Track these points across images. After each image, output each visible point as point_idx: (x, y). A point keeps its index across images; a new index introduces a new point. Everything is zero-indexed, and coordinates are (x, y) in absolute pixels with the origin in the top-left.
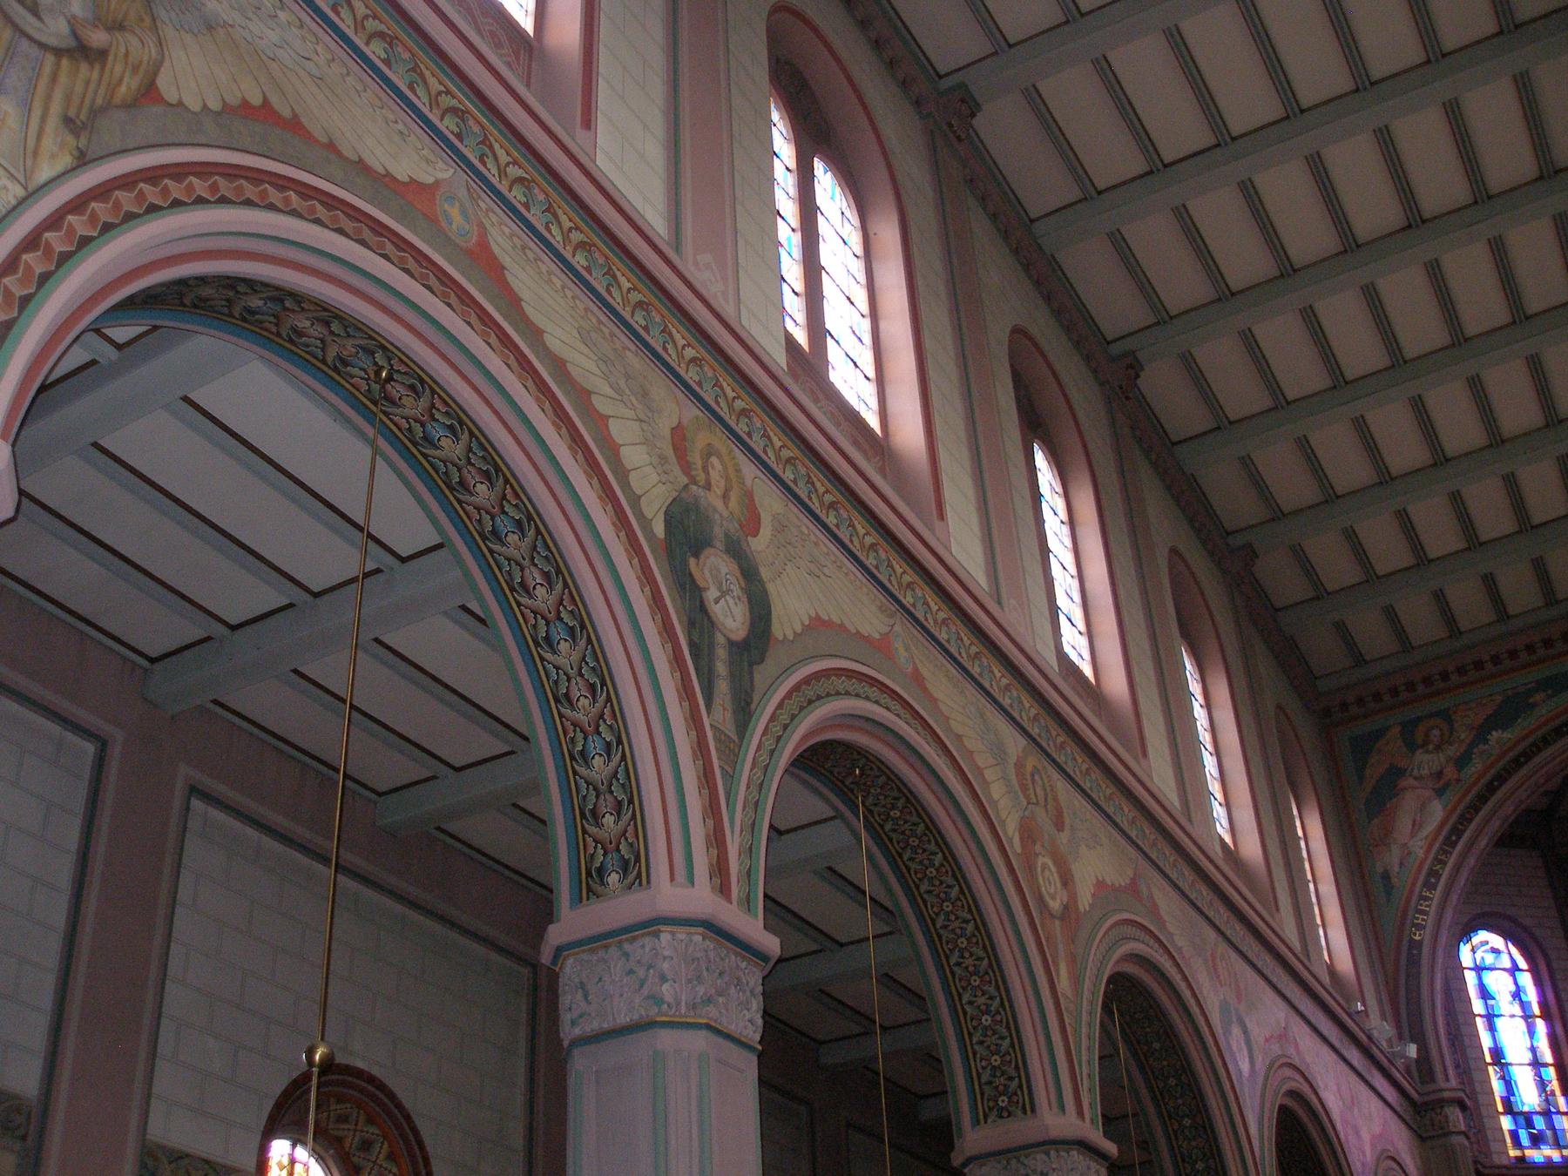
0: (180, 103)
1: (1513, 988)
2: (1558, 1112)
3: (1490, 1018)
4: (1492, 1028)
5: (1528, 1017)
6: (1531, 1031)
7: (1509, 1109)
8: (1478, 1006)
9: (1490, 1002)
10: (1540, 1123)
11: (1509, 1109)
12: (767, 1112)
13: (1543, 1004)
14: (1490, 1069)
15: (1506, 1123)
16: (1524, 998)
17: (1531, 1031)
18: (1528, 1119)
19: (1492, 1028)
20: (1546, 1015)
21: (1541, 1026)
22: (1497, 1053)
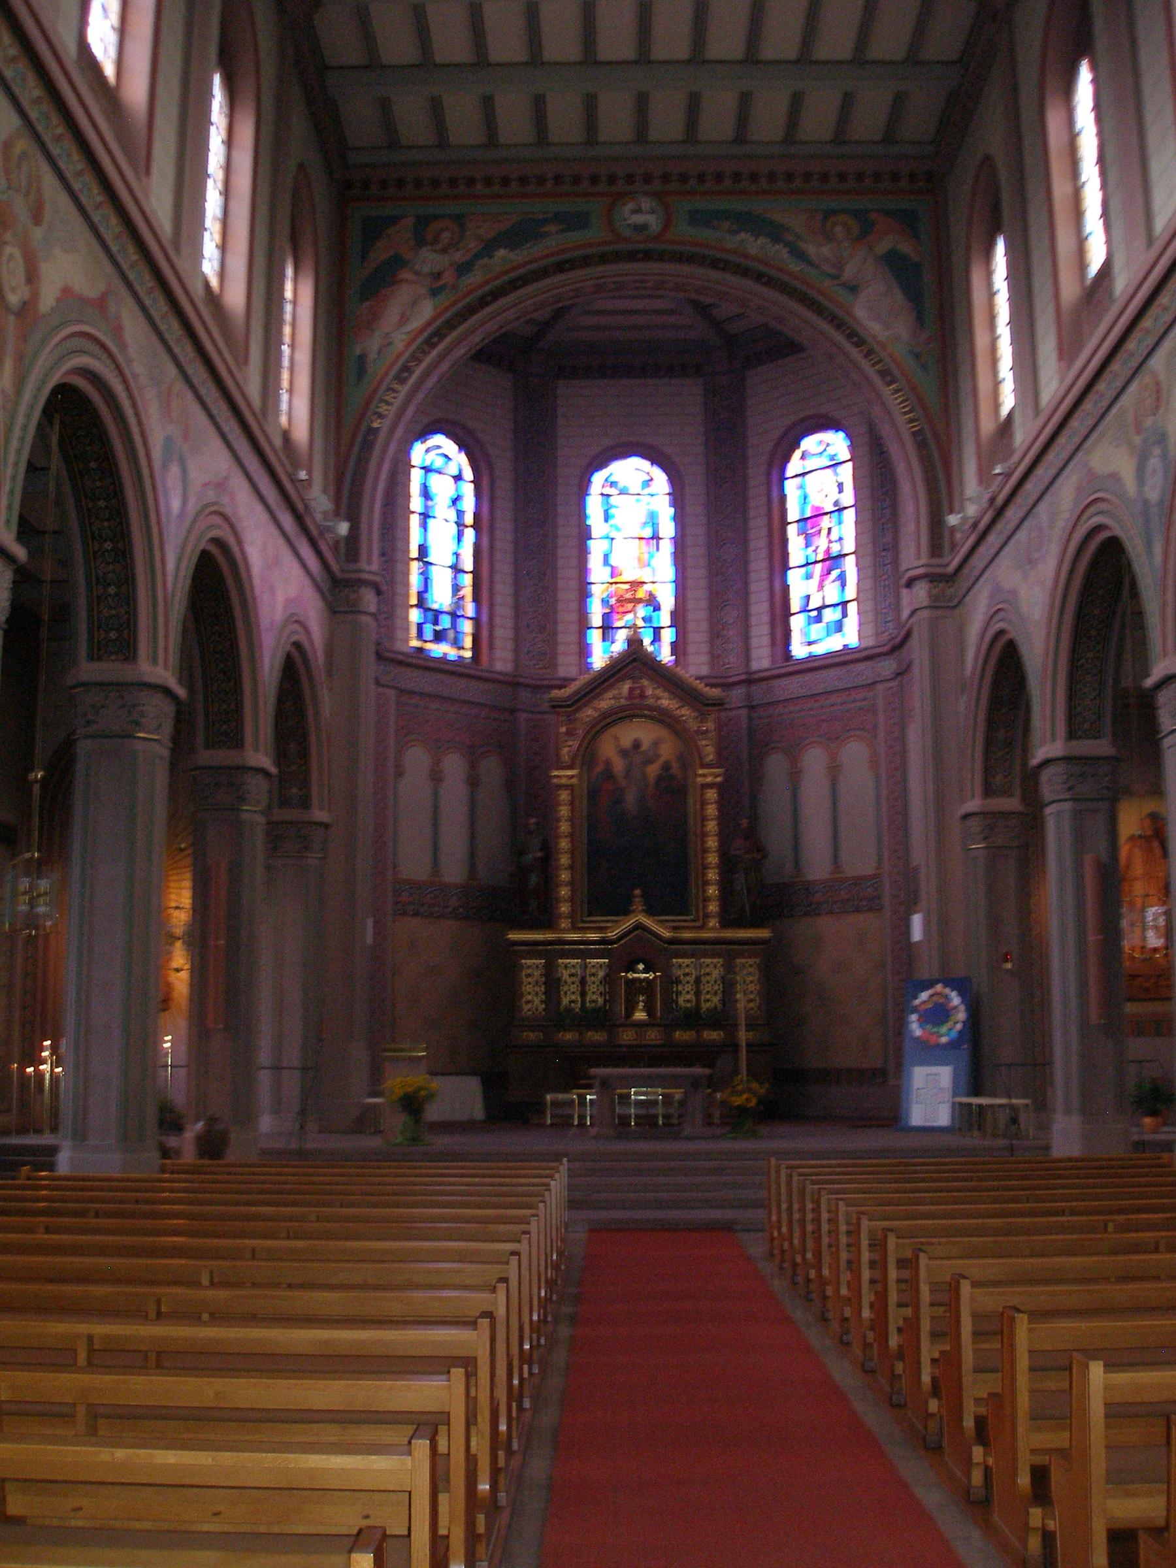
3: (425, 516)
4: (424, 526)
7: (421, 604)
10: (445, 622)
11: (421, 604)
15: (415, 616)
18: (437, 614)
19: (424, 526)
20: (476, 526)
21: (470, 535)
22: (423, 550)
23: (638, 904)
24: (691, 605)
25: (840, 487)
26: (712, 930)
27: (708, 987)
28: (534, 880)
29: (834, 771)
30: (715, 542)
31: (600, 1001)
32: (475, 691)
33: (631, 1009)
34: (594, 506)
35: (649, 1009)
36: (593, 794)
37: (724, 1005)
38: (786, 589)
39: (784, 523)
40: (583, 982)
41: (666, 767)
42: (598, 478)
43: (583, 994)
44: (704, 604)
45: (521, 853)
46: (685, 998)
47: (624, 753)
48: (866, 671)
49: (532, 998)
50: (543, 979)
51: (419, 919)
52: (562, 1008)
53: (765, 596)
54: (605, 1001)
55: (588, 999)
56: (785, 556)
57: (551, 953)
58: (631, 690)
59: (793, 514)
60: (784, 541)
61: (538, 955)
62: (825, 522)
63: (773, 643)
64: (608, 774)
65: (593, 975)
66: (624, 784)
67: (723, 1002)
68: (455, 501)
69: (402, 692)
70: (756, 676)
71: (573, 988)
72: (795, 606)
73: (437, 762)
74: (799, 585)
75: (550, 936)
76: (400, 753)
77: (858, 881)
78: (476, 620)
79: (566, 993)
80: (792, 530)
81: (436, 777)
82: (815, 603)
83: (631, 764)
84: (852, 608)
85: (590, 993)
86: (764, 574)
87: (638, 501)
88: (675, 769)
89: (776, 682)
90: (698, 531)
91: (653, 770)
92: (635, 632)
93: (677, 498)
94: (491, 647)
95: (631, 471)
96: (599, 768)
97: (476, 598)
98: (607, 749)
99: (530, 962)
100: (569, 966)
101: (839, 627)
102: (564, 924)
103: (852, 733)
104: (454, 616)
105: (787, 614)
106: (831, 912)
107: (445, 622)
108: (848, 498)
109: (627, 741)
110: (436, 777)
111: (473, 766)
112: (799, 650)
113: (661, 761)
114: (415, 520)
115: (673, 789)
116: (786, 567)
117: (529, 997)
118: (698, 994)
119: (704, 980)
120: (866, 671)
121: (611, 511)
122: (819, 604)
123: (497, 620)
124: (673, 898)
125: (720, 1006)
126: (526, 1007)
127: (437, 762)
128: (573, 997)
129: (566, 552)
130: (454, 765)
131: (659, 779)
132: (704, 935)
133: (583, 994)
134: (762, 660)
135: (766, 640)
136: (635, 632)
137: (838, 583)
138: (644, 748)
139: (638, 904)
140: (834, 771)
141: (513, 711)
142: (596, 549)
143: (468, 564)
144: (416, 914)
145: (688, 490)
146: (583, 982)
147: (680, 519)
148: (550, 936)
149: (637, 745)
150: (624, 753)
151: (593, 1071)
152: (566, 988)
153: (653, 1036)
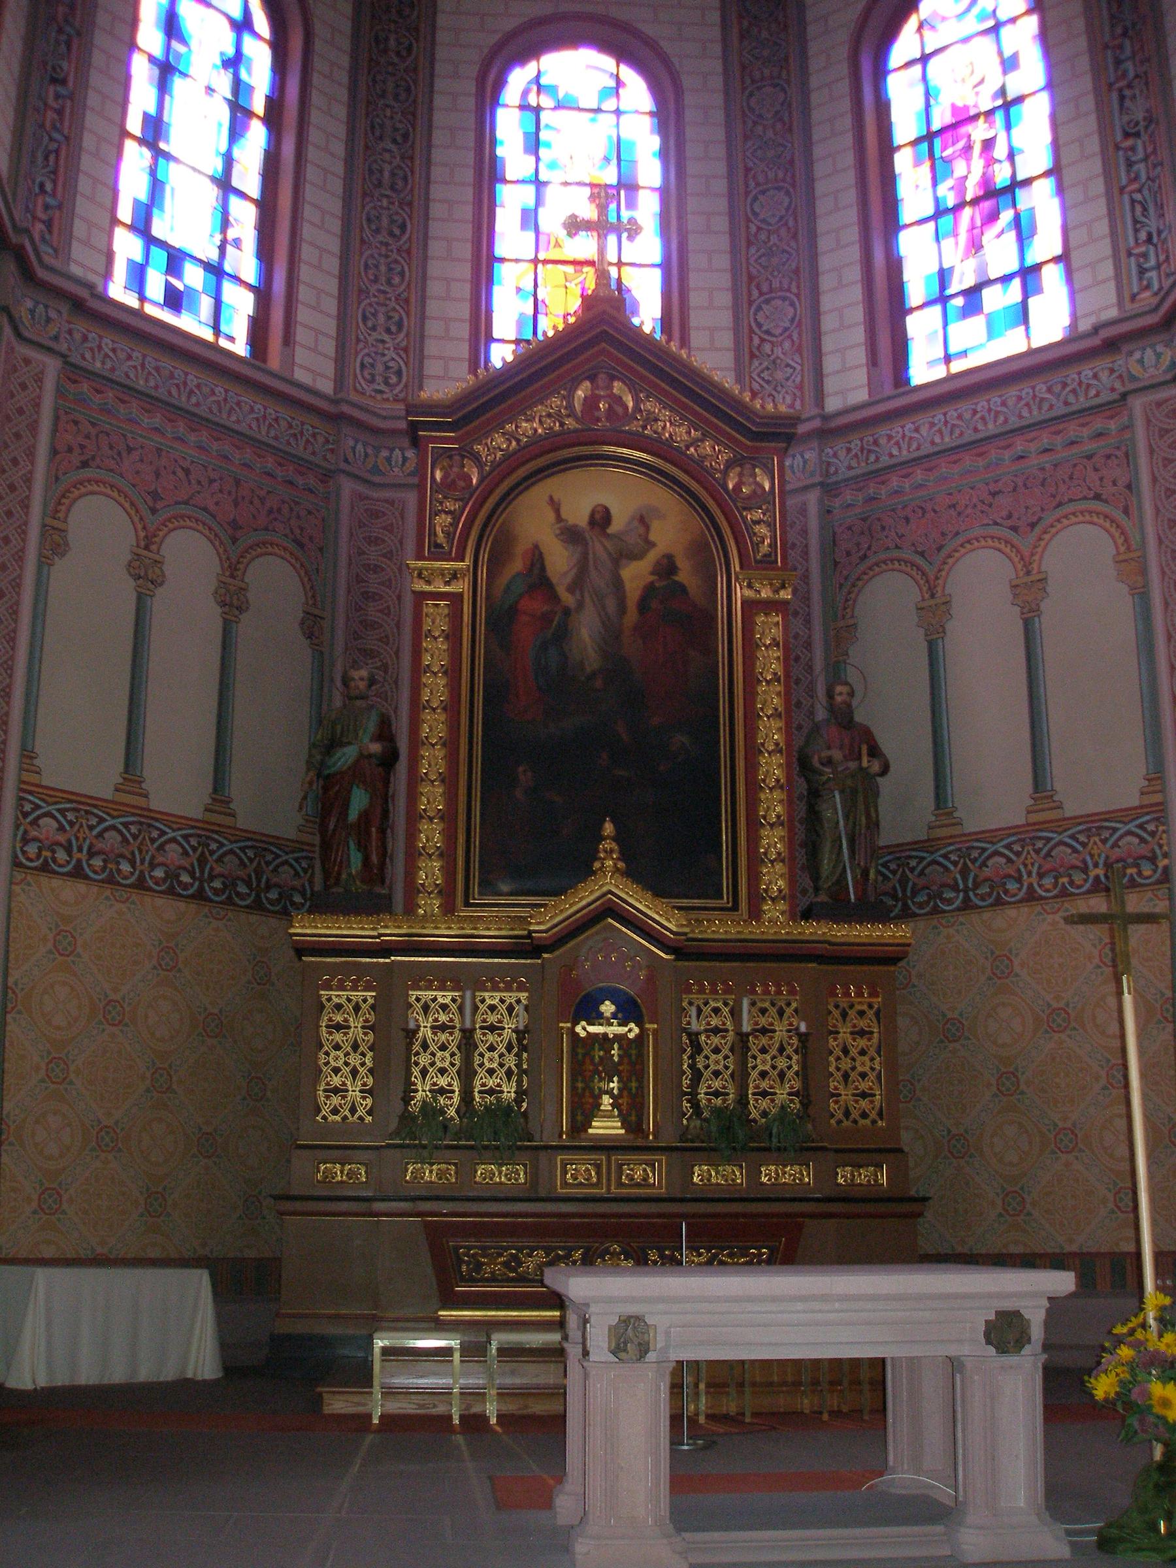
0: (802, 1412)
1: (231, 52)
2: (236, 279)
3: (166, 70)
4: (163, 87)
5: (239, 114)
6: (236, 132)
7: (142, 227)
8: (150, 37)
9: (175, 45)
10: (193, 277)
11: (142, 227)
12: (797, 1363)
13: (274, 104)
14: (130, 146)
15: (127, 246)
16: (244, 75)
17: (236, 132)
18: (175, 260)
19: (163, 87)
20: (273, 118)
21: (257, 135)
22: (155, 128)
23: (609, 857)
24: (696, 299)
25: (1009, 64)
26: (775, 922)
27: (763, 1063)
28: (359, 800)
29: (1029, 594)
30: (744, 187)
31: (509, 1092)
32: (249, 413)
33: (584, 1110)
34: (508, 126)
35: (631, 1110)
36: (501, 621)
37: (805, 1105)
38: (895, 266)
39: (887, 149)
40: (468, 1043)
41: (667, 567)
42: (518, 79)
43: (467, 1074)
44: (725, 299)
45: (332, 745)
46: (715, 1086)
47: (571, 535)
48: (1100, 378)
49: (345, 1085)
50: (371, 1037)
51: (81, 887)
52: (415, 1106)
53: (854, 273)
54: (520, 1093)
55: (477, 1083)
56: (891, 204)
57: (391, 977)
58: (591, 403)
59: (905, 124)
60: (889, 179)
61: (360, 978)
62: (979, 132)
63: (873, 360)
64: (538, 578)
65: (492, 1028)
66: (568, 599)
67: (804, 1095)
68: (234, 62)
69: (73, 372)
70: (833, 424)
71: (443, 1059)
72: (916, 287)
73: (149, 541)
74: (919, 255)
75: (391, 931)
76: (58, 507)
77: (1096, 824)
78: (262, 294)
79: (424, 1072)
80: (903, 161)
81: (146, 574)
82: (965, 278)
83: (585, 556)
84: (1053, 276)
85: (481, 1073)
86: (852, 234)
87: (593, 120)
88: (685, 575)
89: (882, 431)
90: (710, 167)
91: (636, 575)
92: (602, 277)
93: (669, 117)
94: (288, 339)
95: (576, 69)
96: (517, 565)
97: (265, 252)
98: (535, 522)
99: (338, 996)
100: (433, 1007)
101: (1022, 315)
102: (429, 904)
103: (1070, 508)
104: (216, 271)
105: (898, 309)
106: (1031, 897)
107: (193, 277)
108: (1032, 72)
109: (578, 512)
110: (146, 574)
111: (233, 568)
112: (923, 370)
113: (652, 556)
114: (141, 71)
115: (679, 617)
116: (892, 224)
117: (336, 1081)
118: (741, 1077)
119: (754, 1044)
120: (1100, 378)
121: (543, 135)
122: (969, 282)
123: (304, 293)
124: (685, 848)
125: (796, 1106)
126: (328, 1104)
127: (149, 541)
128: (443, 1082)
129: (449, 194)
130: (190, 557)
131: (649, 591)
132: (754, 931)
133: (467, 1074)
134: (848, 385)
135: (860, 356)
136: (602, 277)
137: (1012, 235)
138: (615, 527)
139: (609, 857)
140: (1029, 594)
141: (326, 476)
142: (511, 201)
143: (249, 178)
144: (78, 873)
145: (689, 99)
146: (468, 1043)
147: (674, 153)
148: (391, 931)
149: (601, 519)
150: (571, 535)
151: (580, 1286)
152: (424, 1060)
153: (648, 1174)
